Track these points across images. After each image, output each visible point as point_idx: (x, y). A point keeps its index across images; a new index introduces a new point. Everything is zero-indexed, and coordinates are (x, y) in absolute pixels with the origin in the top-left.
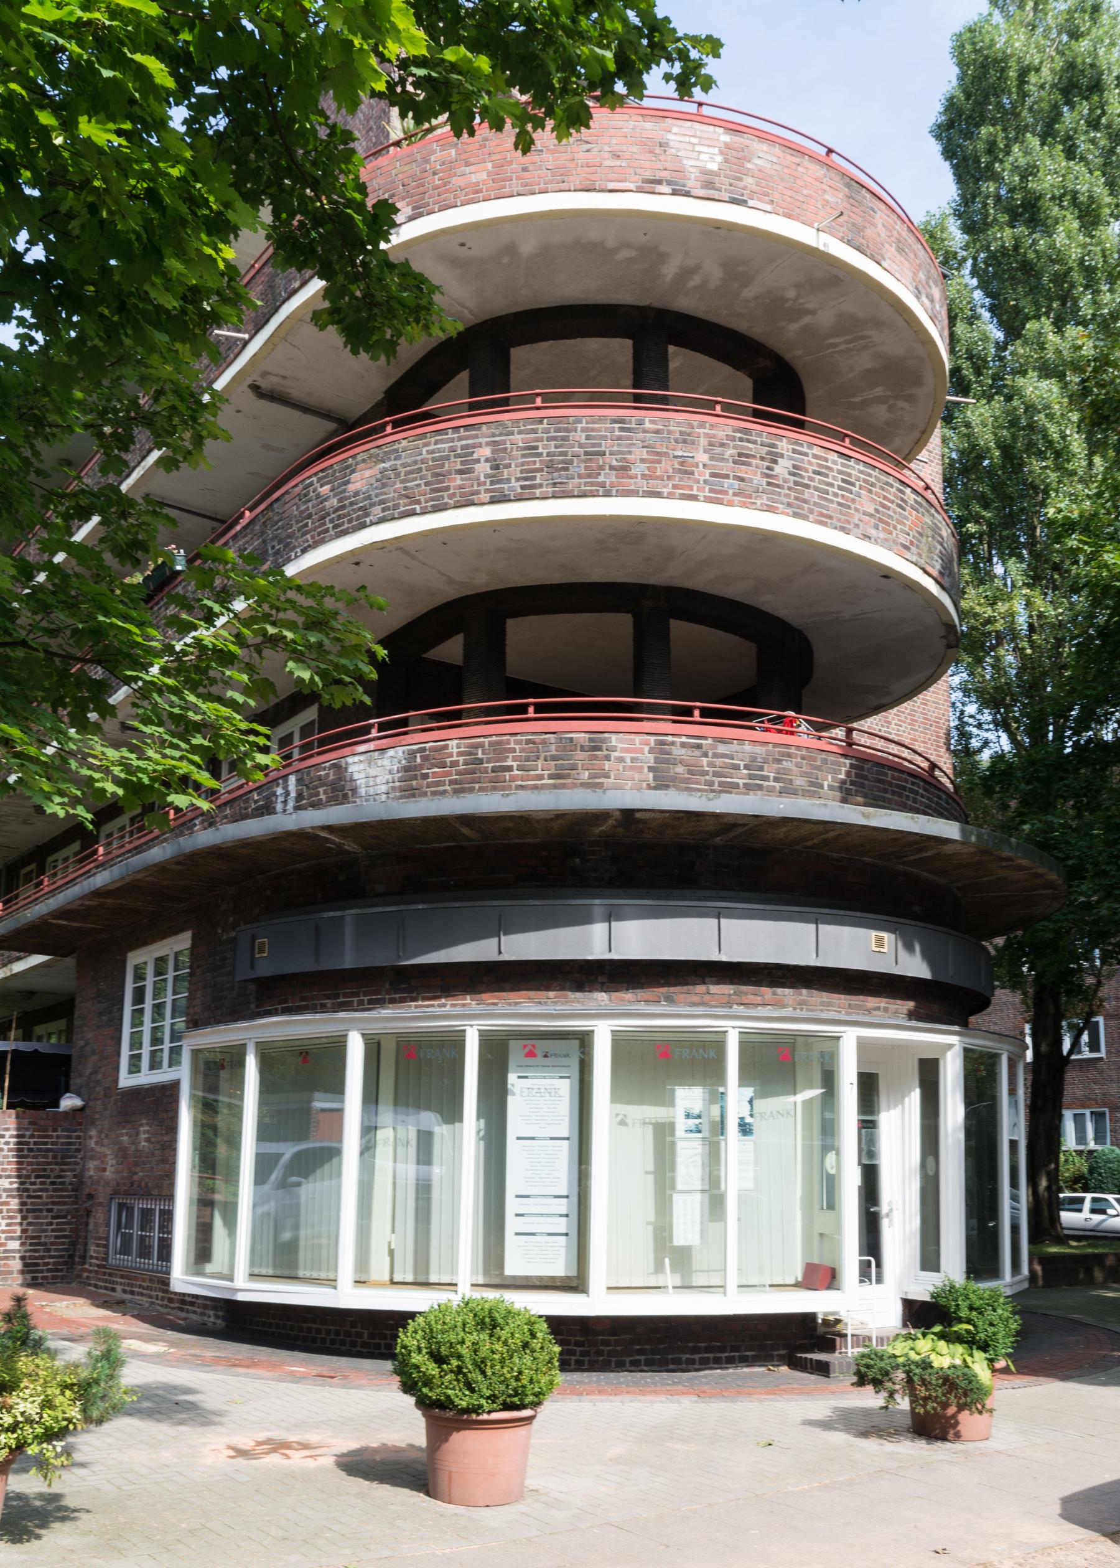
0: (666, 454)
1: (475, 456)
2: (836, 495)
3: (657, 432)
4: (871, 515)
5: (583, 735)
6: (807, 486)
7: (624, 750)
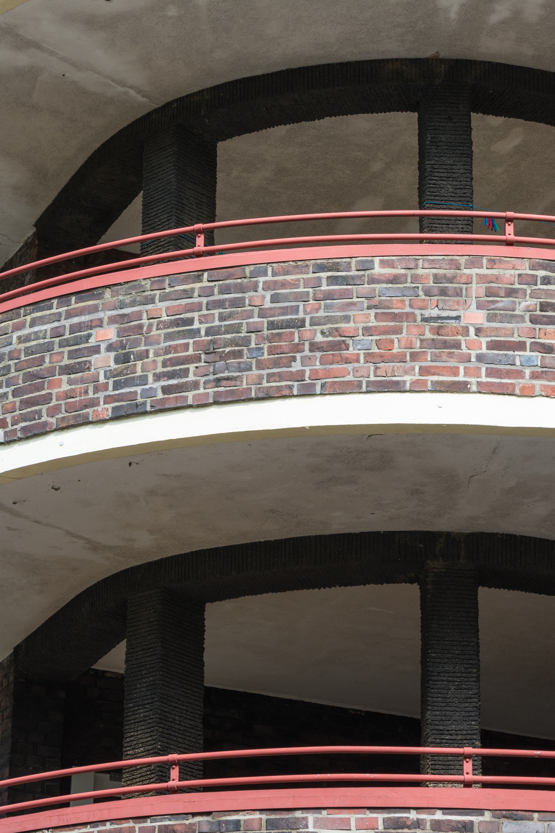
1: (92, 342)
3: (395, 280)
5: (257, 816)
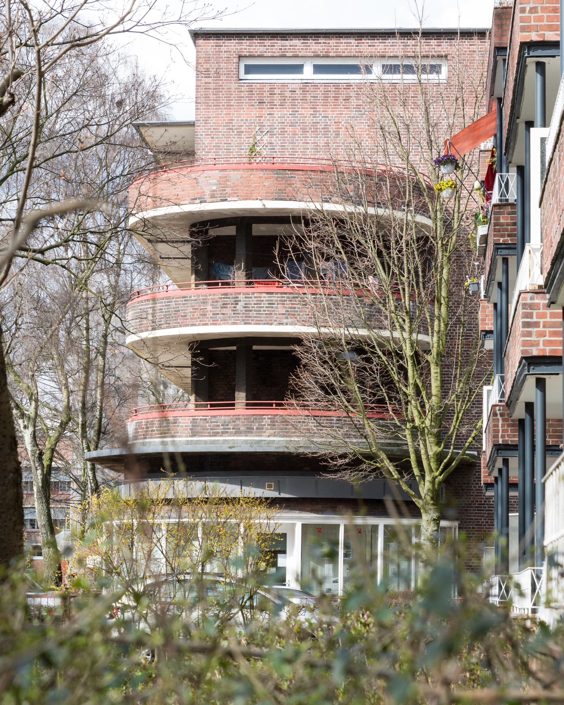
0: (197, 309)
2: (265, 311)
3: (195, 300)
4: (283, 314)
6: (251, 311)
7: (183, 423)
